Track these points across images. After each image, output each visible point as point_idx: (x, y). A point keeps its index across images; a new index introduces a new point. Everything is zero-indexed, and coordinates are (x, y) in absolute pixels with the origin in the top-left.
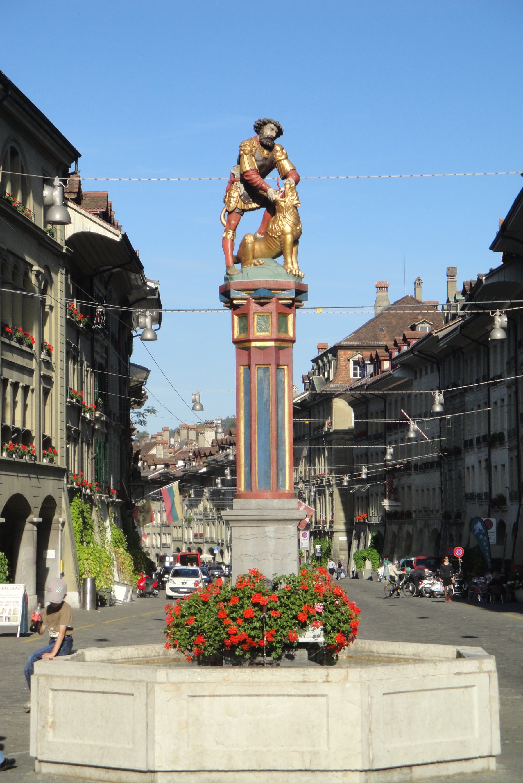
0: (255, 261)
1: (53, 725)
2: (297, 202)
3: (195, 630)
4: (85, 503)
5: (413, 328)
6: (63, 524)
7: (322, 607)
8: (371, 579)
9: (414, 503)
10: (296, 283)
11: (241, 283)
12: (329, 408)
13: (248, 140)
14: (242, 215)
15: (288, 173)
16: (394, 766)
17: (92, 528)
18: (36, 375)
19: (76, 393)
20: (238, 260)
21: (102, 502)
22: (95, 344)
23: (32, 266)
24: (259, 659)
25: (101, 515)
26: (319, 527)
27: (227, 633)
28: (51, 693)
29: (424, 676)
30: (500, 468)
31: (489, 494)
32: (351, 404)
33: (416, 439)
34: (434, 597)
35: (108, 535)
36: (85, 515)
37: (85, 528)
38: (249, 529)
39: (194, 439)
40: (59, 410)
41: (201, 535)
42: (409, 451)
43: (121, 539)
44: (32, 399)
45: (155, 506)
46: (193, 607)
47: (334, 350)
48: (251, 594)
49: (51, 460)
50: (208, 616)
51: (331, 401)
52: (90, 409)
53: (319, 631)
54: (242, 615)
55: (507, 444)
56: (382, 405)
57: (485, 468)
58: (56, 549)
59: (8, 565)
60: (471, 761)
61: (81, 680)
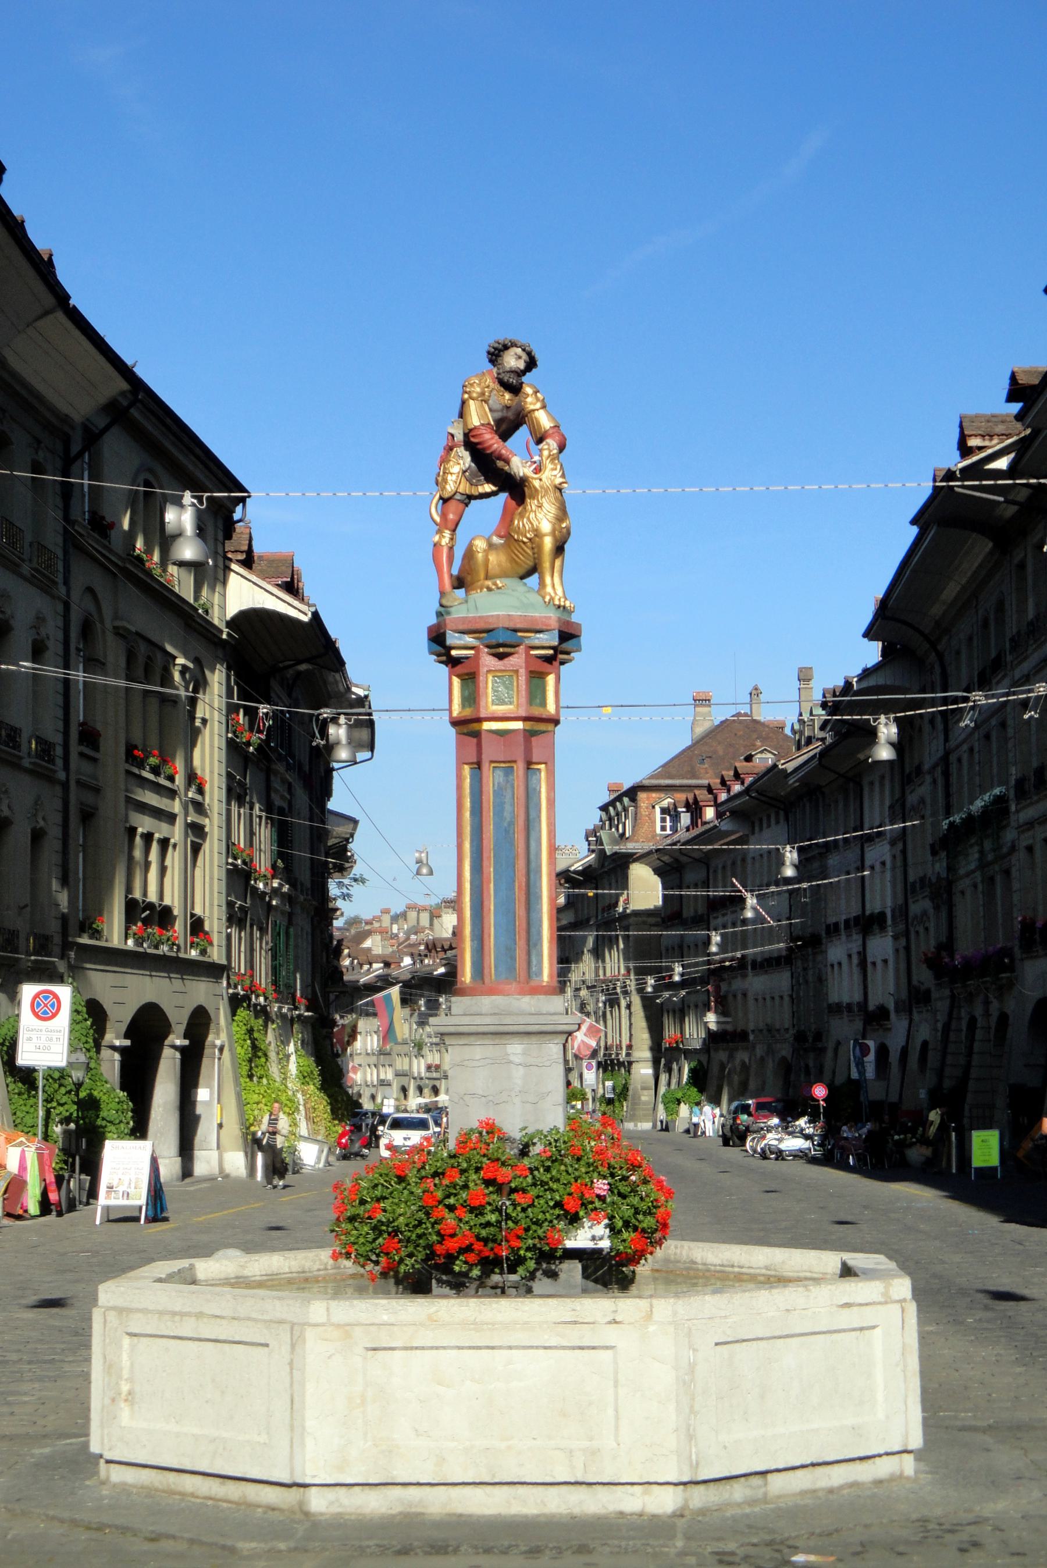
0: (489, 583)
1: (130, 1398)
2: (561, 480)
3: (384, 1228)
4: (256, 1017)
5: (749, 759)
6: (221, 1049)
7: (606, 1187)
8: (688, 1131)
9: (752, 1019)
10: (559, 620)
11: (464, 619)
12: (626, 877)
13: (476, 376)
14: (467, 505)
15: (546, 432)
16: (734, 1473)
17: (266, 1055)
18: (179, 822)
19: (243, 851)
20: (459, 583)
21: (283, 1017)
22: (272, 778)
23: (175, 658)
24: (496, 1278)
25: (280, 1035)
26: (611, 1055)
27: (438, 1233)
28: (126, 1341)
29: (788, 1310)
30: (880, 965)
31: (863, 1005)
32: (658, 871)
33: (754, 921)
34: (783, 1159)
35: (293, 1067)
36: (256, 1035)
37: (255, 1055)
38: (478, 1049)
39: (428, 925)
40: (216, 876)
41: (438, 1067)
42: (743, 940)
43: (312, 1072)
44: (174, 859)
45: (363, 1024)
46: (380, 1187)
47: (632, 793)
48: (481, 1162)
49: (203, 952)
50: (406, 1203)
51: (628, 868)
52: (265, 876)
53: (601, 1229)
54: (465, 1201)
55: (890, 929)
56: (704, 874)
57: (858, 966)
58: (209, 1086)
59: (132, 1111)
60: (870, 1461)
61: (177, 1318)
